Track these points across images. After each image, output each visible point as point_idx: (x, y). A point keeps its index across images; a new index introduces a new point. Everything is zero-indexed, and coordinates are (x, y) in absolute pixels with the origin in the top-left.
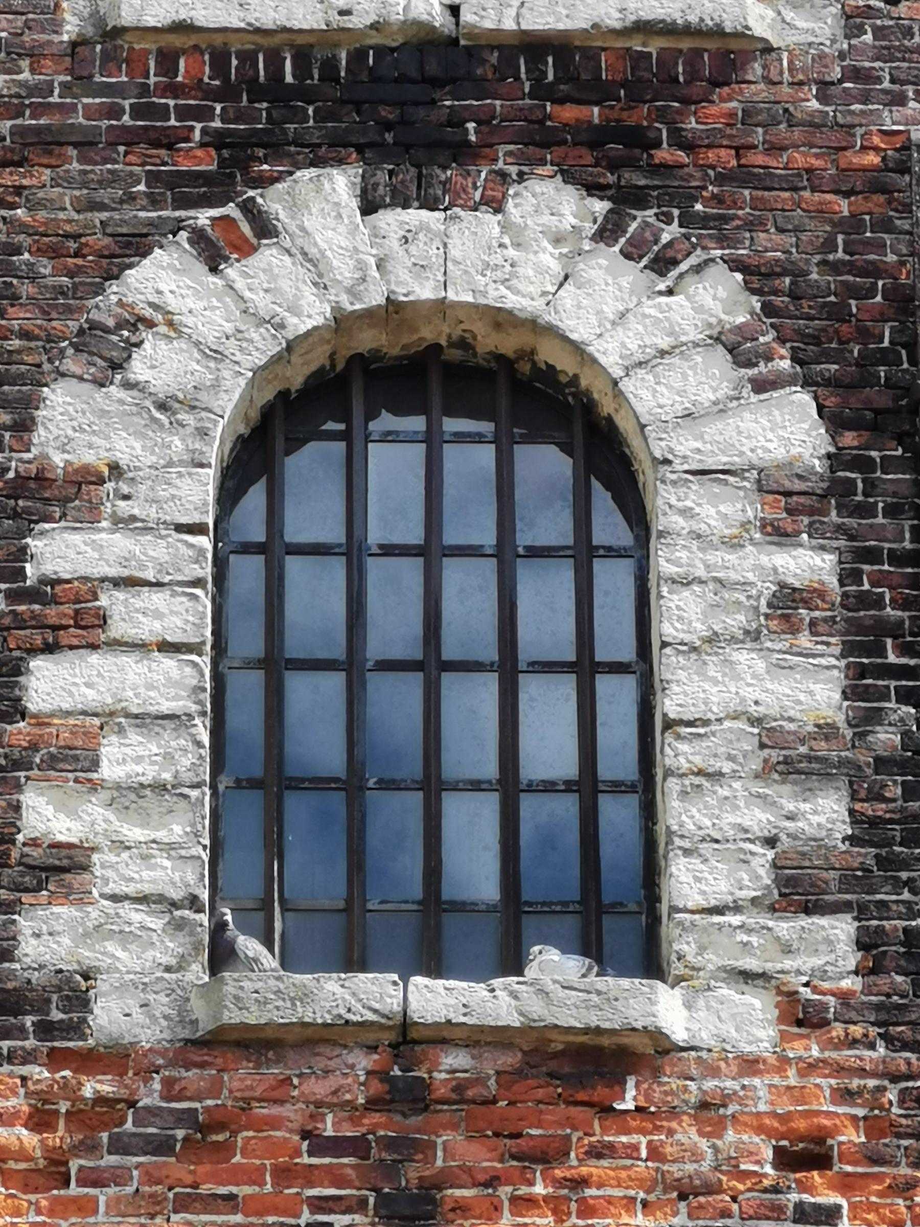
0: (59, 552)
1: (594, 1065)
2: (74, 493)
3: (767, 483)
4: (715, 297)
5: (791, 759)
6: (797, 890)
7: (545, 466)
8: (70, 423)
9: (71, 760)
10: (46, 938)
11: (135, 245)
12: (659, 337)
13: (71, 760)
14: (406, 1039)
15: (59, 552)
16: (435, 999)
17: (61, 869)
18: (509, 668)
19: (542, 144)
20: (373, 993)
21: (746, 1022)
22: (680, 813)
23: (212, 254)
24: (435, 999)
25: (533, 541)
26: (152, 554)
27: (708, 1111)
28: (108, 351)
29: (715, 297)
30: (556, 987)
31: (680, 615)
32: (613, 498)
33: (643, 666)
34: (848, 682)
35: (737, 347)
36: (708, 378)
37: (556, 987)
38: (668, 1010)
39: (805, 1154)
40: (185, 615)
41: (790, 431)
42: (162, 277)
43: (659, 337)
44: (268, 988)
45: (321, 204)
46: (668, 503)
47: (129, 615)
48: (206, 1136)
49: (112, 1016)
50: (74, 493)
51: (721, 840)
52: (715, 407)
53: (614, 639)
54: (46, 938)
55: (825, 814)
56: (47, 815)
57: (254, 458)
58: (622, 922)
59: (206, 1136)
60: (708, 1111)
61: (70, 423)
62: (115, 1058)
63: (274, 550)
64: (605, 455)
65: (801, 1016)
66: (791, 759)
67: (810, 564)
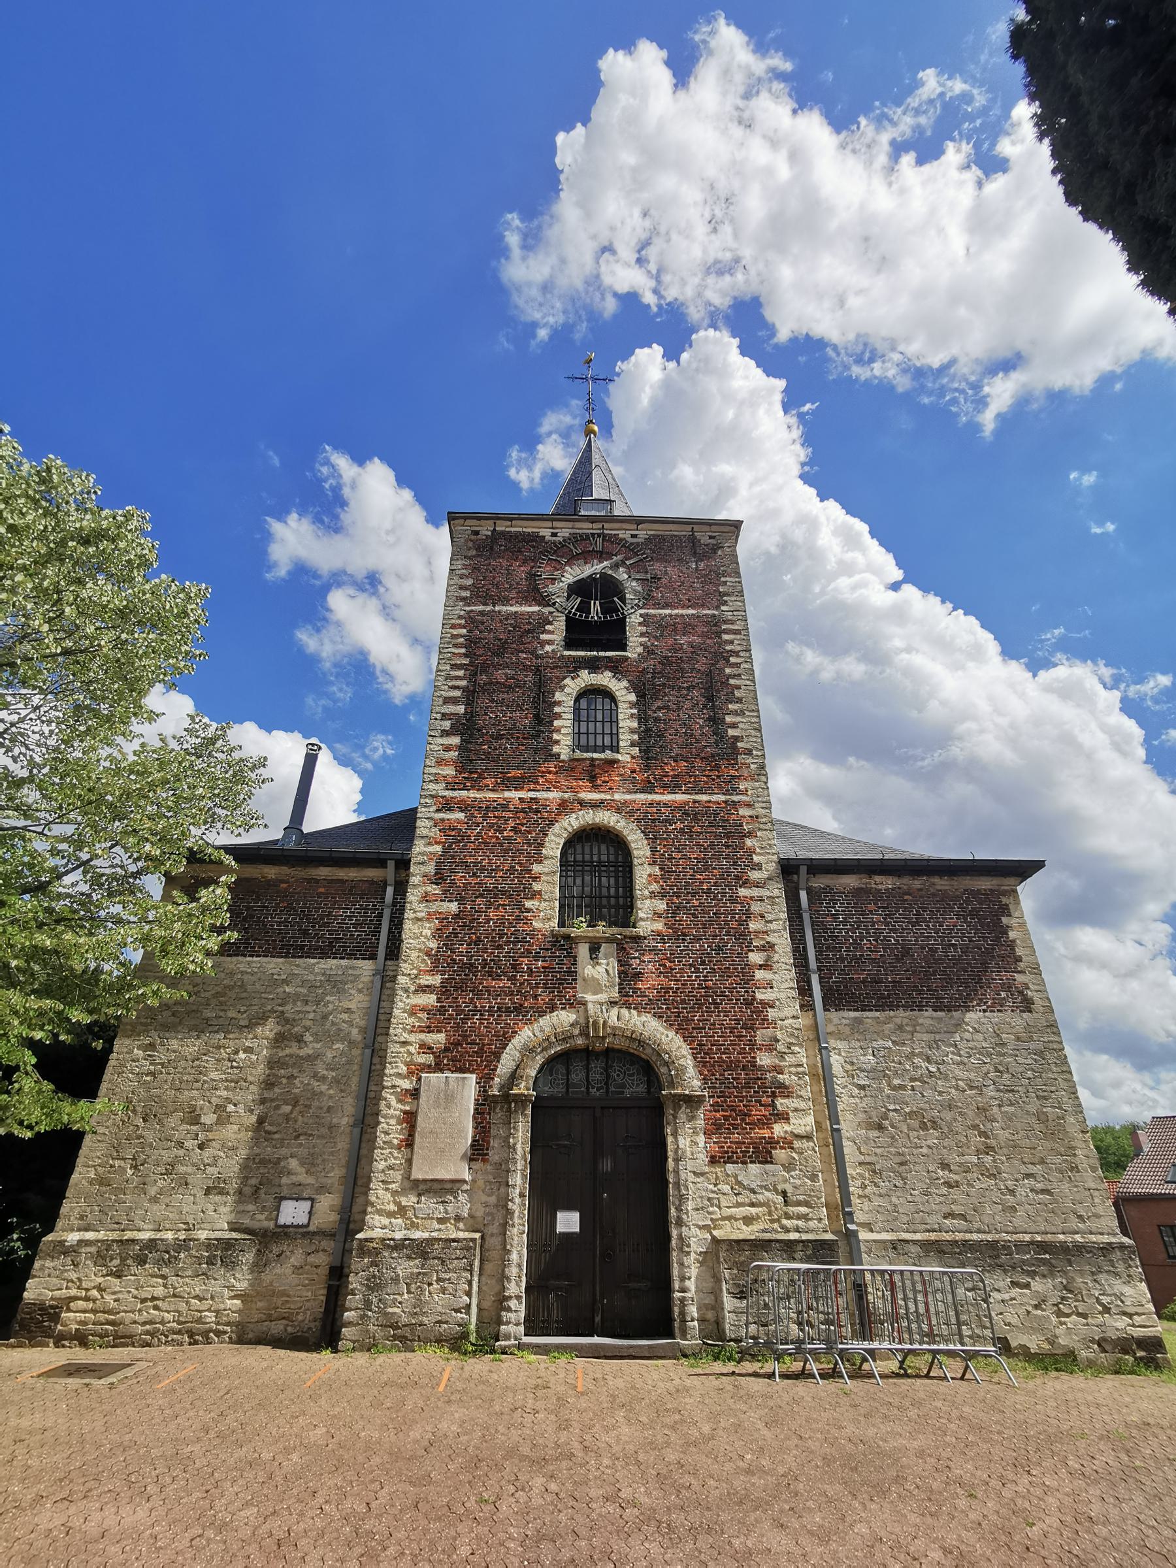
0: (557, 709)
1: (612, 762)
2: (559, 703)
3: (630, 703)
4: (625, 683)
5: (632, 731)
6: (633, 745)
7: (607, 700)
8: (558, 696)
9: (558, 731)
10: (556, 749)
11: (565, 678)
12: (619, 687)
13: (558, 731)
14: (593, 759)
15: (557, 709)
16: (596, 755)
17: (557, 742)
18: (595, 734)
19: (607, 668)
20: (590, 755)
21: (628, 758)
22: (621, 737)
23: (573, 679)
24: (596, 755)
25: (976, 653)
26: (567, 710)
27: (624, 767)
28: (562, 689)
29: (625, 683)
30: (608, 754)
31: (621, 716)
32: (555, 154)
33: (617, 722)
34: (461, 609)
35: (627, 688)
36: (624, 692)
37: (608, 754)
38: (619, 757)
39: (633, 771)
40: (570, 716)
41: (633, 697)
42: (567, 681)
43: (619, 687)
44: (578, 754)
45: (584, 674)
46: (620, 705)
47: (564, 716)
48: (572, 769)
49: (562, 757)
50: (559, 703)
51: (625, 739)
52: (624, 694)
53: (614, 731)
54: (556, 749)
55: (636, 737)
56: (556, 736)
57: (577, 700)
58: (615, 749)
59: (572, 769)
60: (624, 767)
61: (558, 696)
62: (563, 761)
63: (579, 709)
64: (613, 699)
65: (633, 757)
66: (632, 731)
67: (635, 711)
